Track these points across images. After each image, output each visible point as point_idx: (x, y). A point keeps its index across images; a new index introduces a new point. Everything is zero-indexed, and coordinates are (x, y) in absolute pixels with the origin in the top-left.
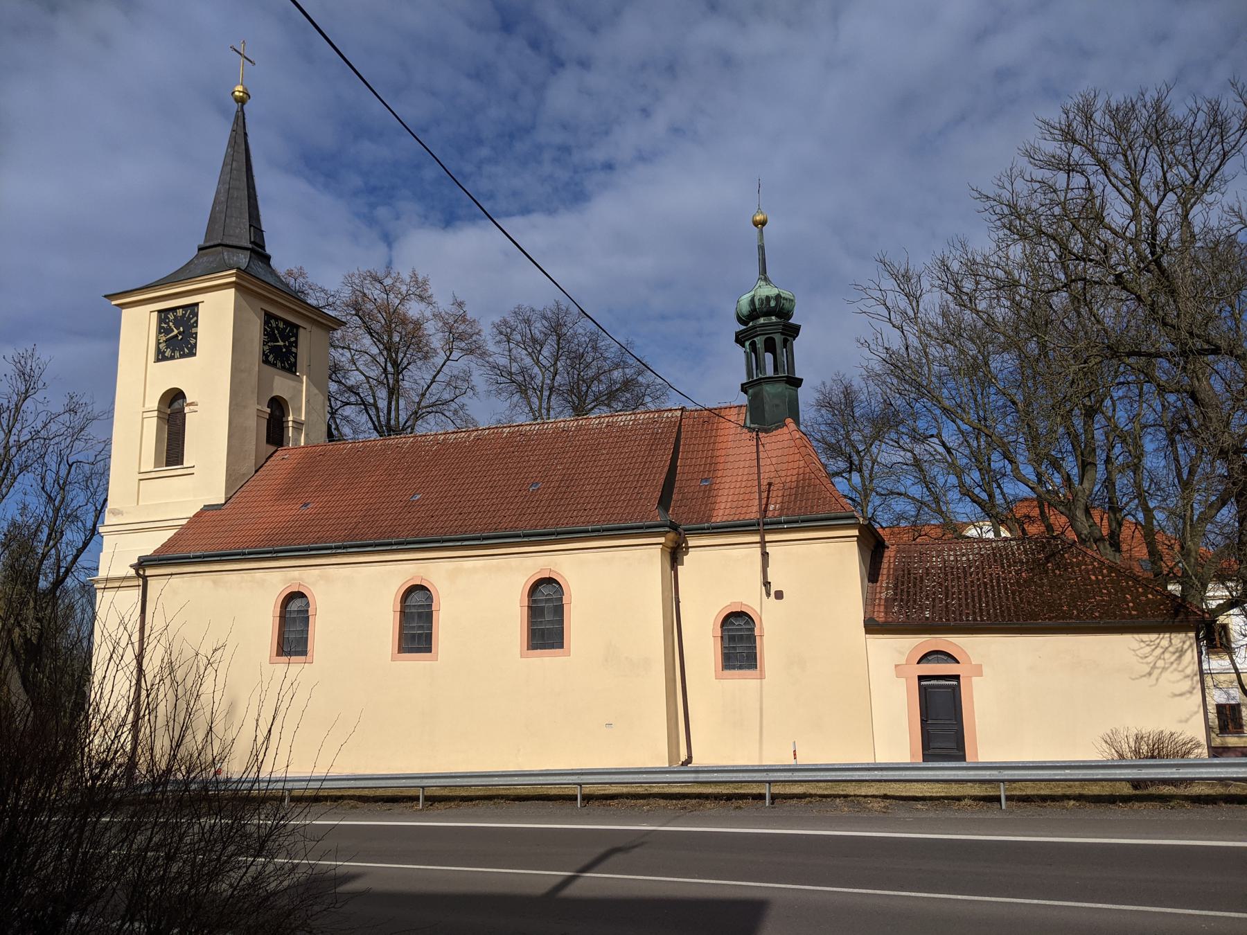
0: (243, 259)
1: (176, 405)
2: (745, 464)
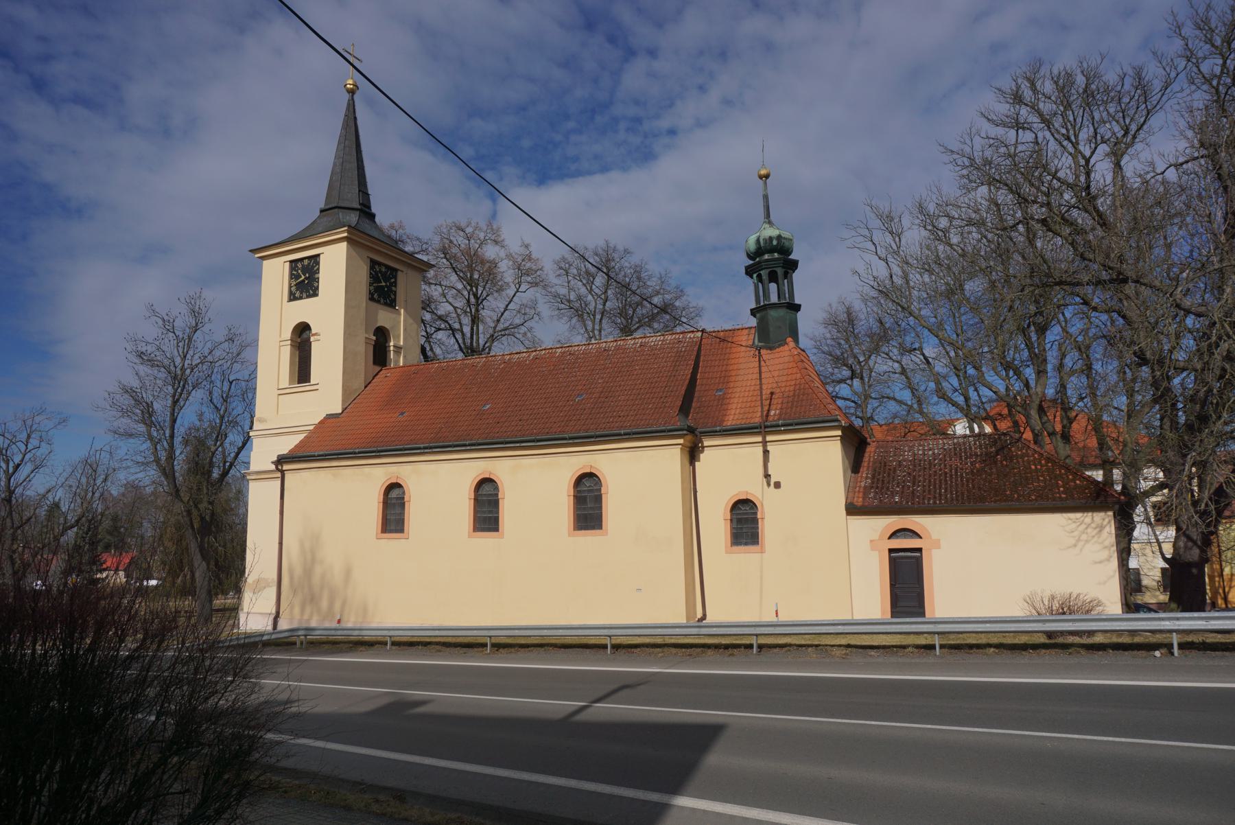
0: (353, 218)
1: (304, 336)
2: (752, 377)
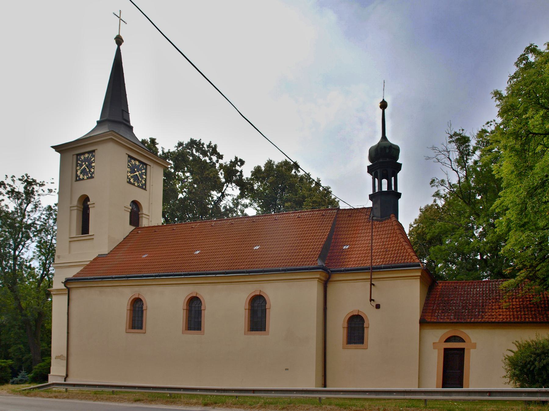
2: (360, 247)
